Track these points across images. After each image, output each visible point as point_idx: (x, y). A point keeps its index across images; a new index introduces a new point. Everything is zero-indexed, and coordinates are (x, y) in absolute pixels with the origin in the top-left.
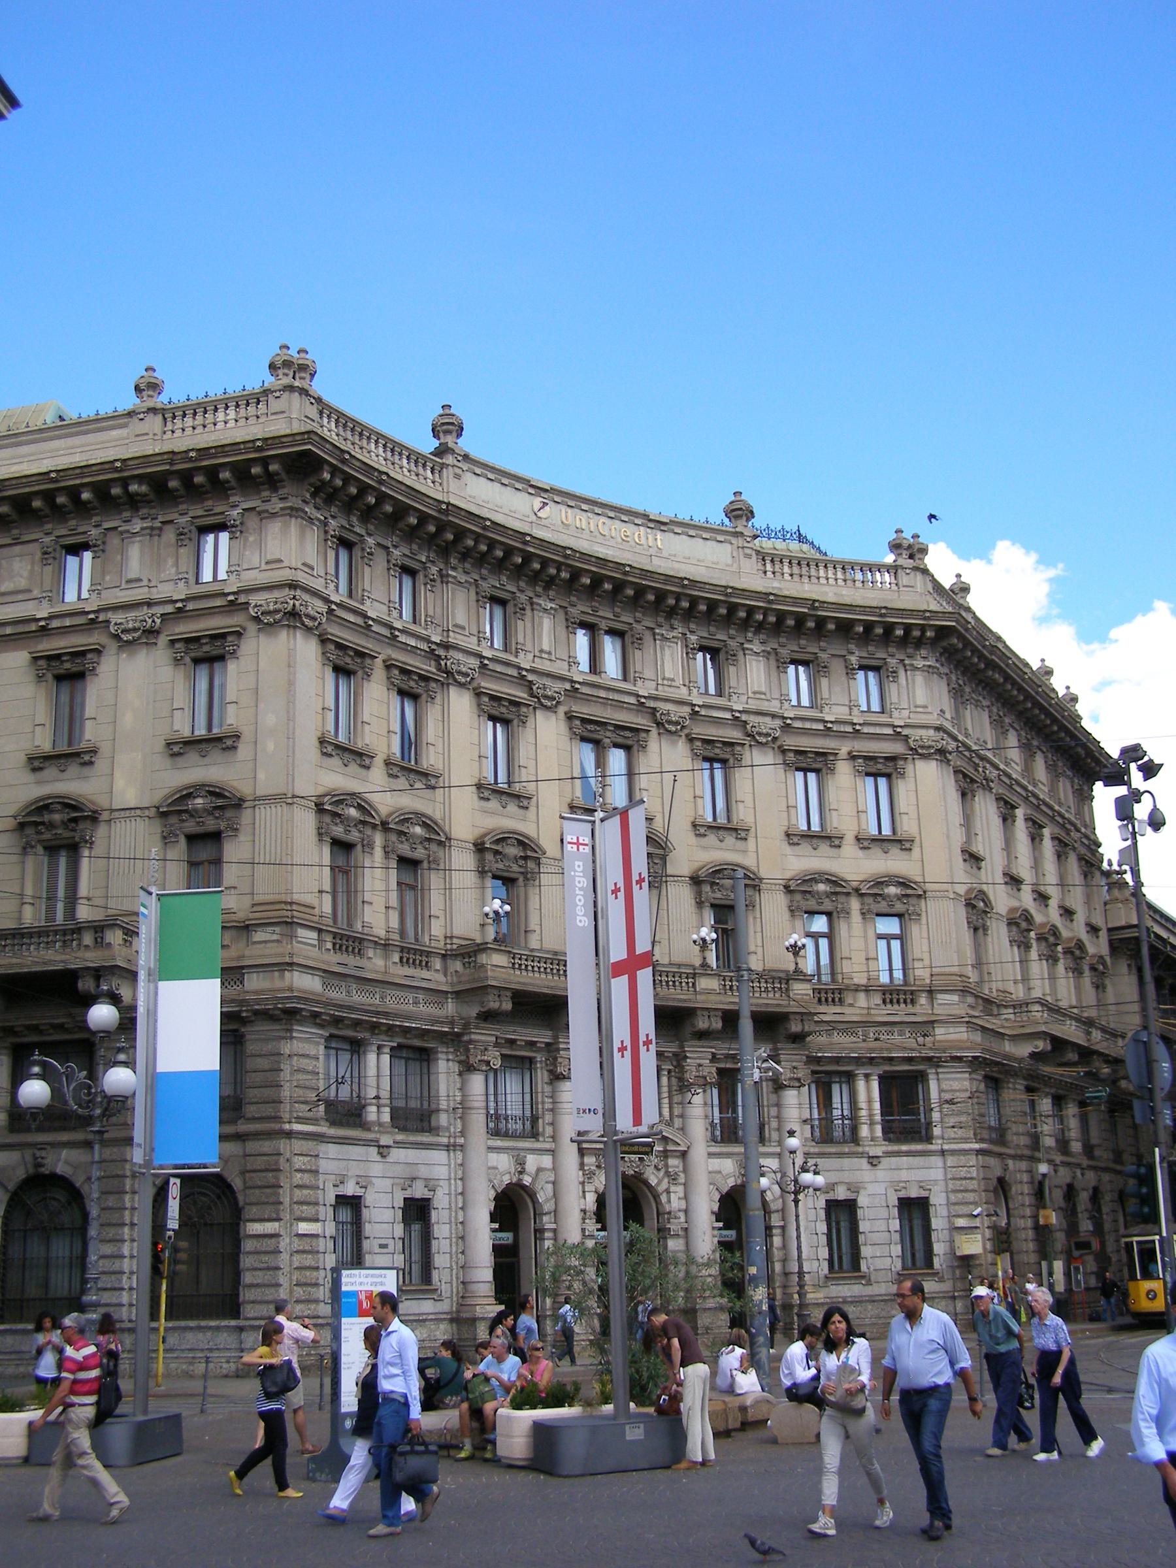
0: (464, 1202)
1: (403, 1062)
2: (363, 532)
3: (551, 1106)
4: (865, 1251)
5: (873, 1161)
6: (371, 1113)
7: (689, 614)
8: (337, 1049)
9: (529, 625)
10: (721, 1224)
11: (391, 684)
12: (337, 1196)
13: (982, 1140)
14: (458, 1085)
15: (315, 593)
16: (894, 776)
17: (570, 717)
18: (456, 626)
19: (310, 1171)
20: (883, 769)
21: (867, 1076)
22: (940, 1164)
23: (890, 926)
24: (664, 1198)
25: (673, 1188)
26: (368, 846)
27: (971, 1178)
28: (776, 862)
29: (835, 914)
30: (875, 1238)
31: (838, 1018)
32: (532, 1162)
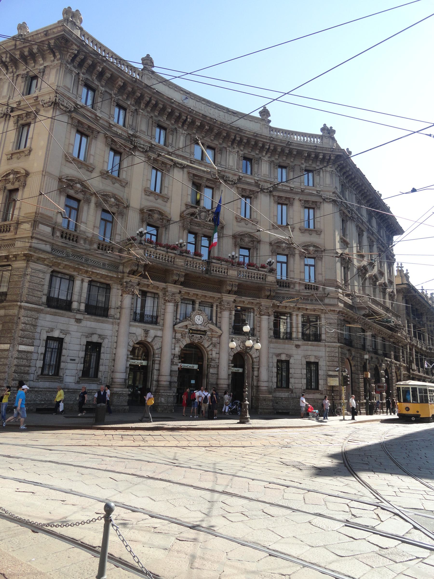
0: (116, 346)
1: (97, 288)
2: (99, 85)
3: (163, 313)
4: (292, 380)
5: (297, 346)
6: (75, 305)
7: (240, 142)
8: (61, 278)
9: (175, 138)
10: (233, 365)
11: (107, 144)
12: (87, 342)
13: (341, 343)
14: (120, 299)
15: (69, 98)
16: (315, 208)
17: (189, 173)
18: (141, 130)
19: (32, 325)
20: (311, 205)
21: (297, 315)
22: (324, 350)
23: (311, 262)
24: (210, 353)
25: (213, 349)
26: (88, 201)
27: (336, 357)
28: (268, 234)
29: (289, 255)
30: (296, 376)
31: (287, 292)
32: (152, 333)
